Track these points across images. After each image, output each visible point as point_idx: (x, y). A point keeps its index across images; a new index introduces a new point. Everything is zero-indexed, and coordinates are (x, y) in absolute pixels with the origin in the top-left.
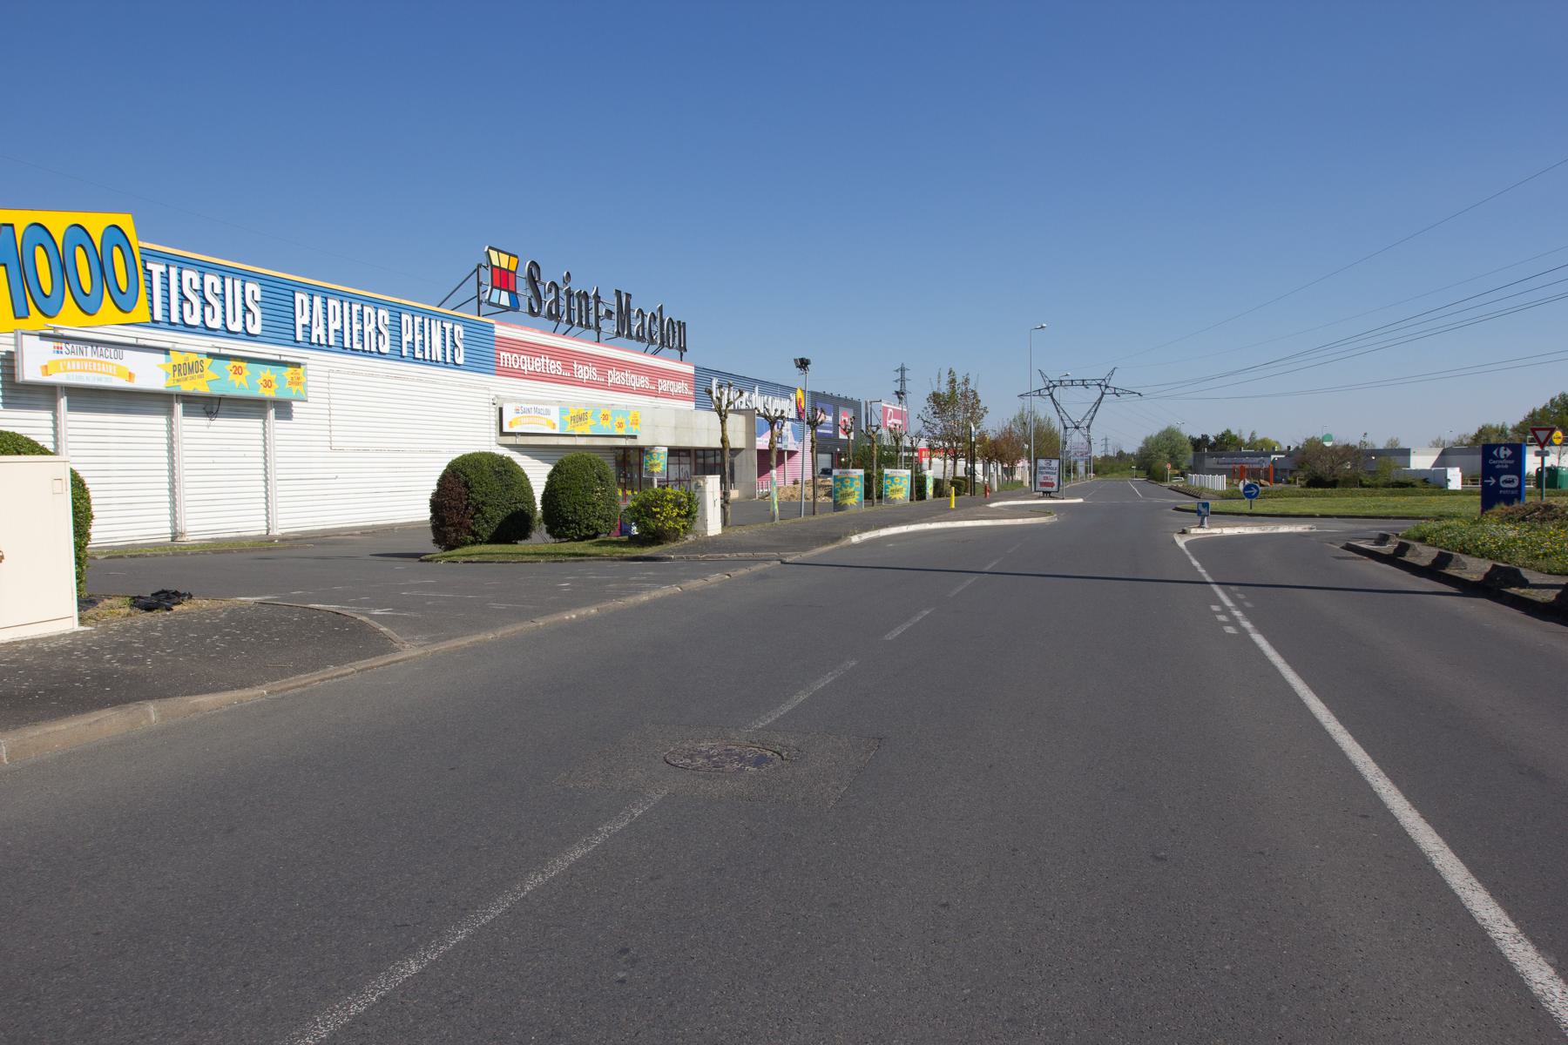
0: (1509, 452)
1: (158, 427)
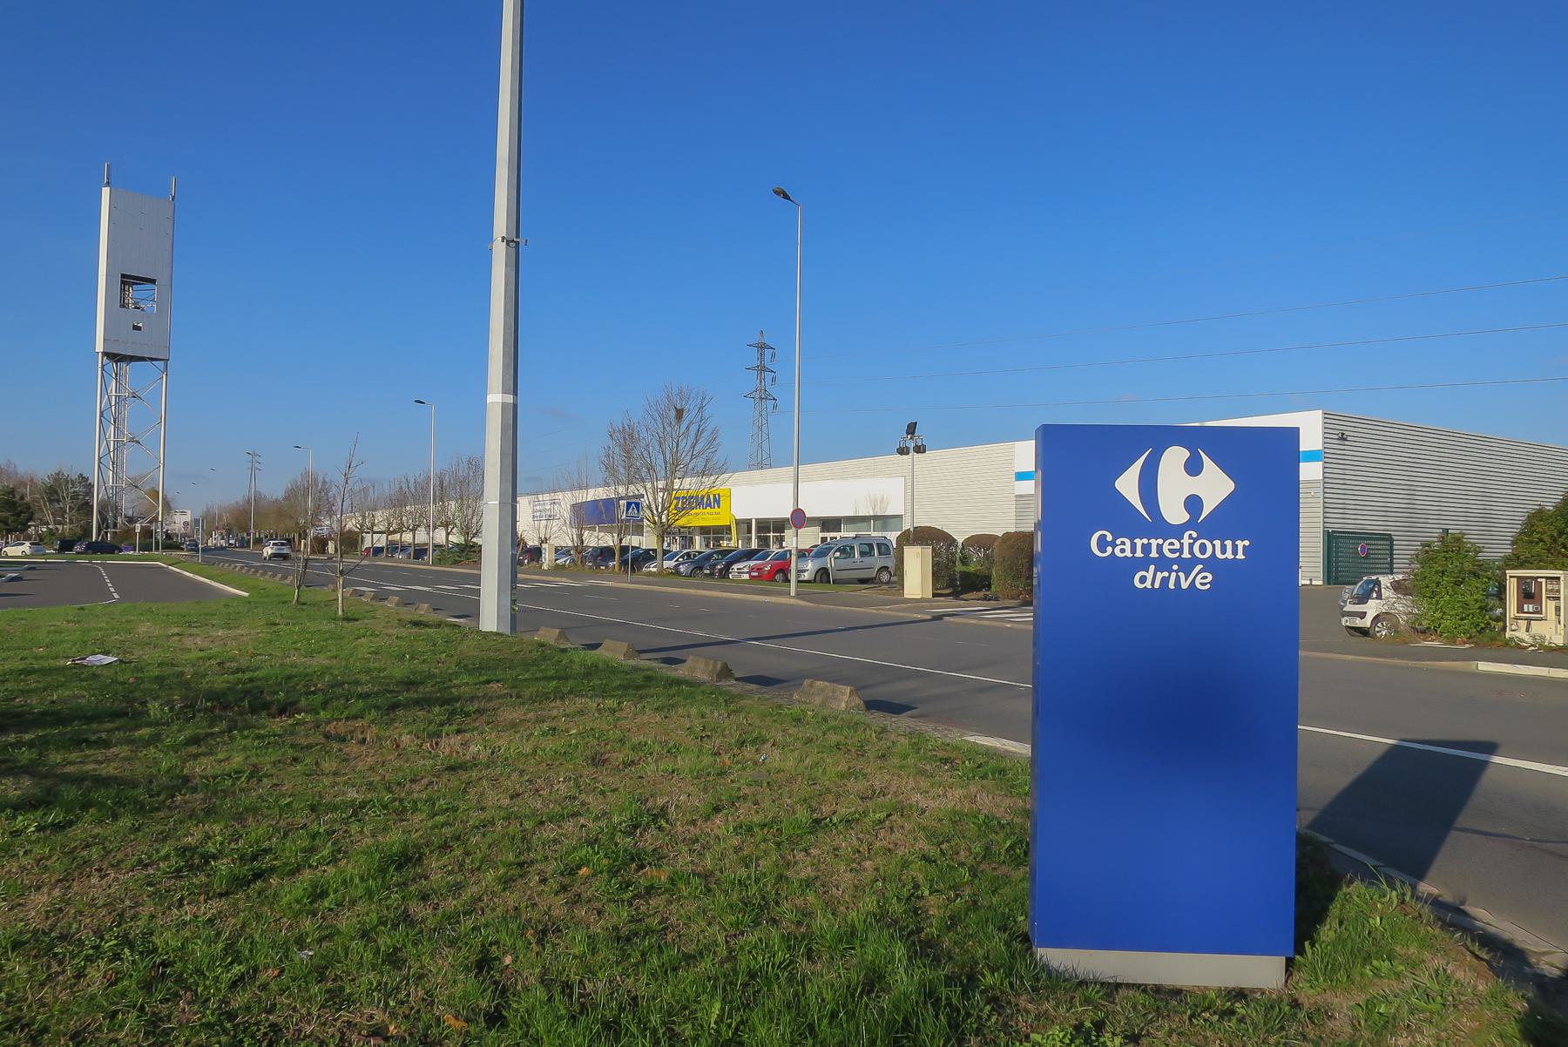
0: (1215, 486)
1: (1306, 540)
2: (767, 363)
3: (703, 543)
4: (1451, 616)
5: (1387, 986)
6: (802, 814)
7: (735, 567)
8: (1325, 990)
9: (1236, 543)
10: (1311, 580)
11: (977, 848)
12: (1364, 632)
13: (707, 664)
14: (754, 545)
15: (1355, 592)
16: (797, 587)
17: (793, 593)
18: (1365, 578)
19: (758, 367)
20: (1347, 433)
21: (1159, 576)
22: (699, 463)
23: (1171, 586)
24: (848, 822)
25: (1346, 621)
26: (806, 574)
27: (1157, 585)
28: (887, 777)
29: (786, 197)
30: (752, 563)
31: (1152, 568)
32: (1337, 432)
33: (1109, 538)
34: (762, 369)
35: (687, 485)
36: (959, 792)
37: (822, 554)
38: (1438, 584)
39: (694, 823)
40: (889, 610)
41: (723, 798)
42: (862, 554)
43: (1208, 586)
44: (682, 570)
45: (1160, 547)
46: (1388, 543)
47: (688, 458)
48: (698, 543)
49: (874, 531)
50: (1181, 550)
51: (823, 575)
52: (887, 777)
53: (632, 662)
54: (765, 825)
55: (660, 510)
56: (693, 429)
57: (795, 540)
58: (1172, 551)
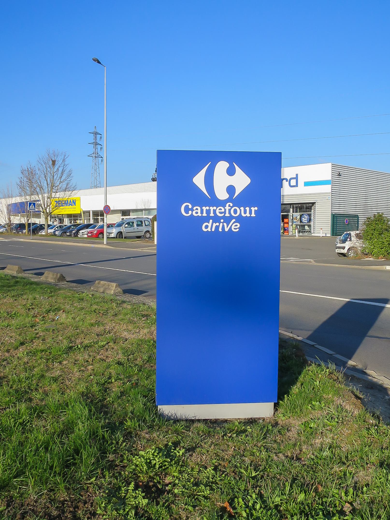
2: (98, 141)
3: (69, 222)
4: (377, 247)
5: (317, 414)
6: (65, 343)
7: (81, 232)
8: (290, 417)
9: (251, 209)
10: (326, 234)
11: (145, 357)
12: (344, 255)
13: (53, 275)
14: (92, 222)
15: (341, 238)
16: (107, 240)
17: (105, 243)
18: (345, 233)
19: (94, 143)
20: (341, 173)
21: (214, 225)
22: (64, 185)
23: (220, 230)
24: (86, 347)
25: (338, 251)
26: (112, 234)
27: (213, 230)
28: (114, 325)
29: (99, 62)
30: (89, 230)
31: (211, 221)
32: (337, 172)
33: (190, 207)
34: (96, 144)
35: (60, 195)
36: (146, 331)
37: (120, 225)
38: (372, 234)
39: (8, 351)
40: (147, 249)
41: (28, 338)
42: (138, 225)
43: (238, 230)
44: (57, 233)
45: (215, 211)
46: (356, 218)
47: (58, 183)
48: (66, 222)
49: (145, 215)
50: (225, 213)
51: (120, 234)
52: (114, 325)
53: (20, 275)
54: (43, 351)
55: (46, 207)
56: (61, 169)
57: (110, 219)
58: (221, 213)
